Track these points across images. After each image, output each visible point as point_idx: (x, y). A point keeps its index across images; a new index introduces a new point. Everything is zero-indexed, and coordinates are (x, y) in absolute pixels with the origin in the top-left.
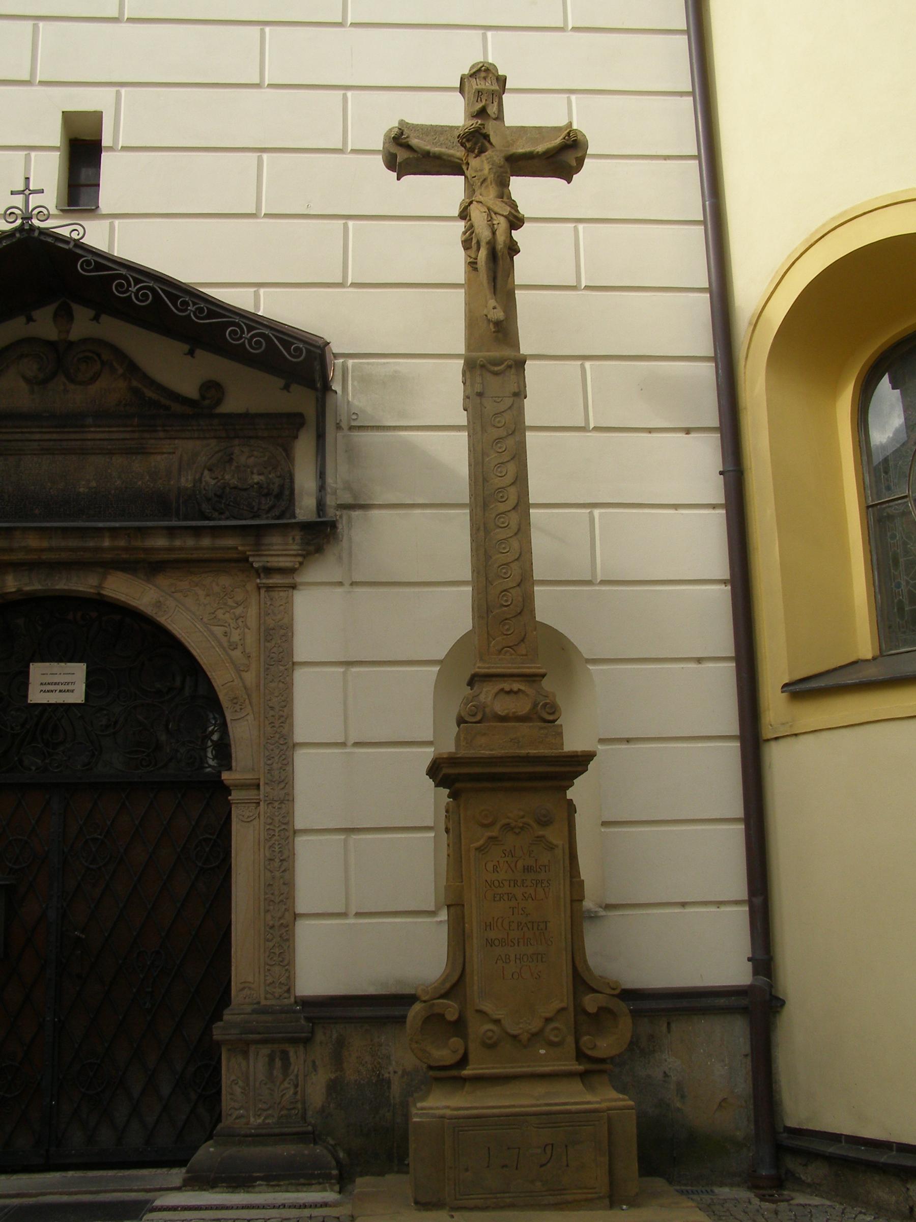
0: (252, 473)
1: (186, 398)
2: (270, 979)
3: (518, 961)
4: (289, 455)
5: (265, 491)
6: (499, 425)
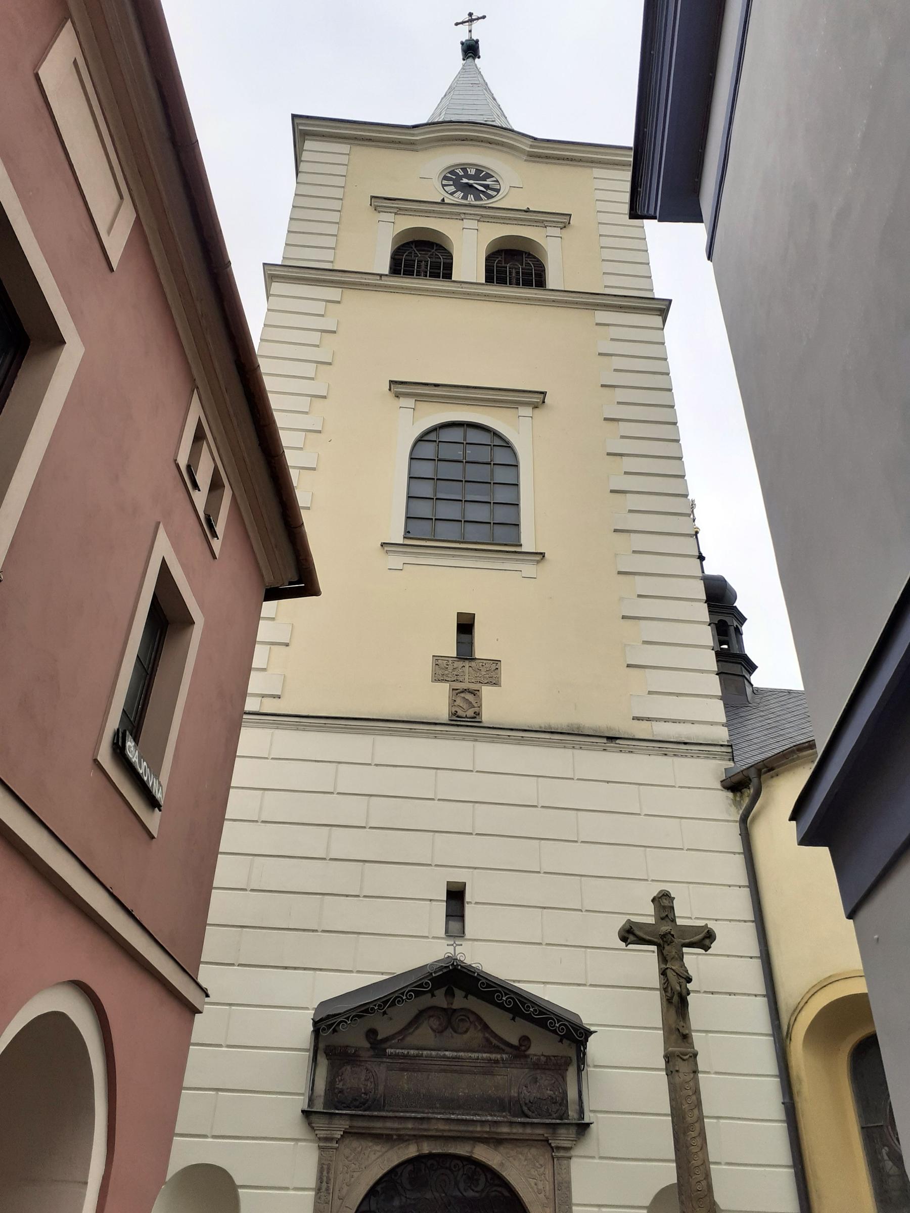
1: (512, 1044)
4: (564, 1078)
5: (555, 1100)
6: (688, 1088)
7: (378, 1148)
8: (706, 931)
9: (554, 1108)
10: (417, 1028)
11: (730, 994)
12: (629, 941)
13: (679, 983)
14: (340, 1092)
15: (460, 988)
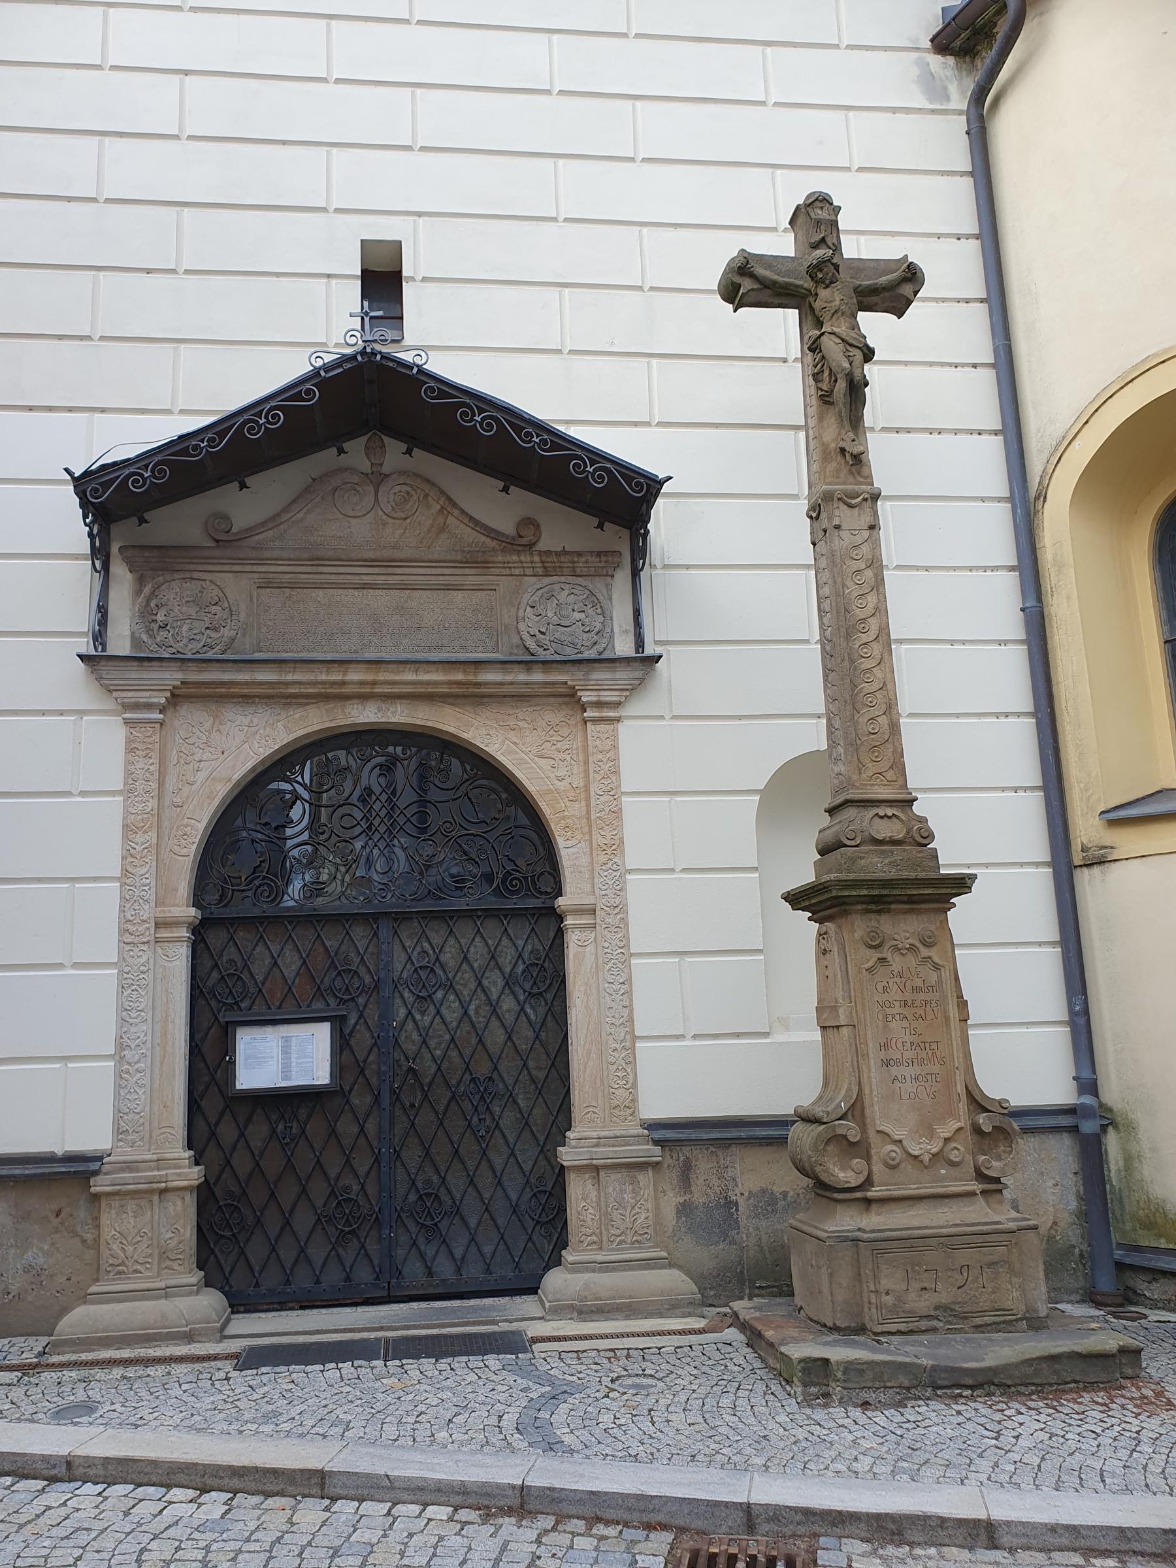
3: (914, 1081)
11: (931, 431)
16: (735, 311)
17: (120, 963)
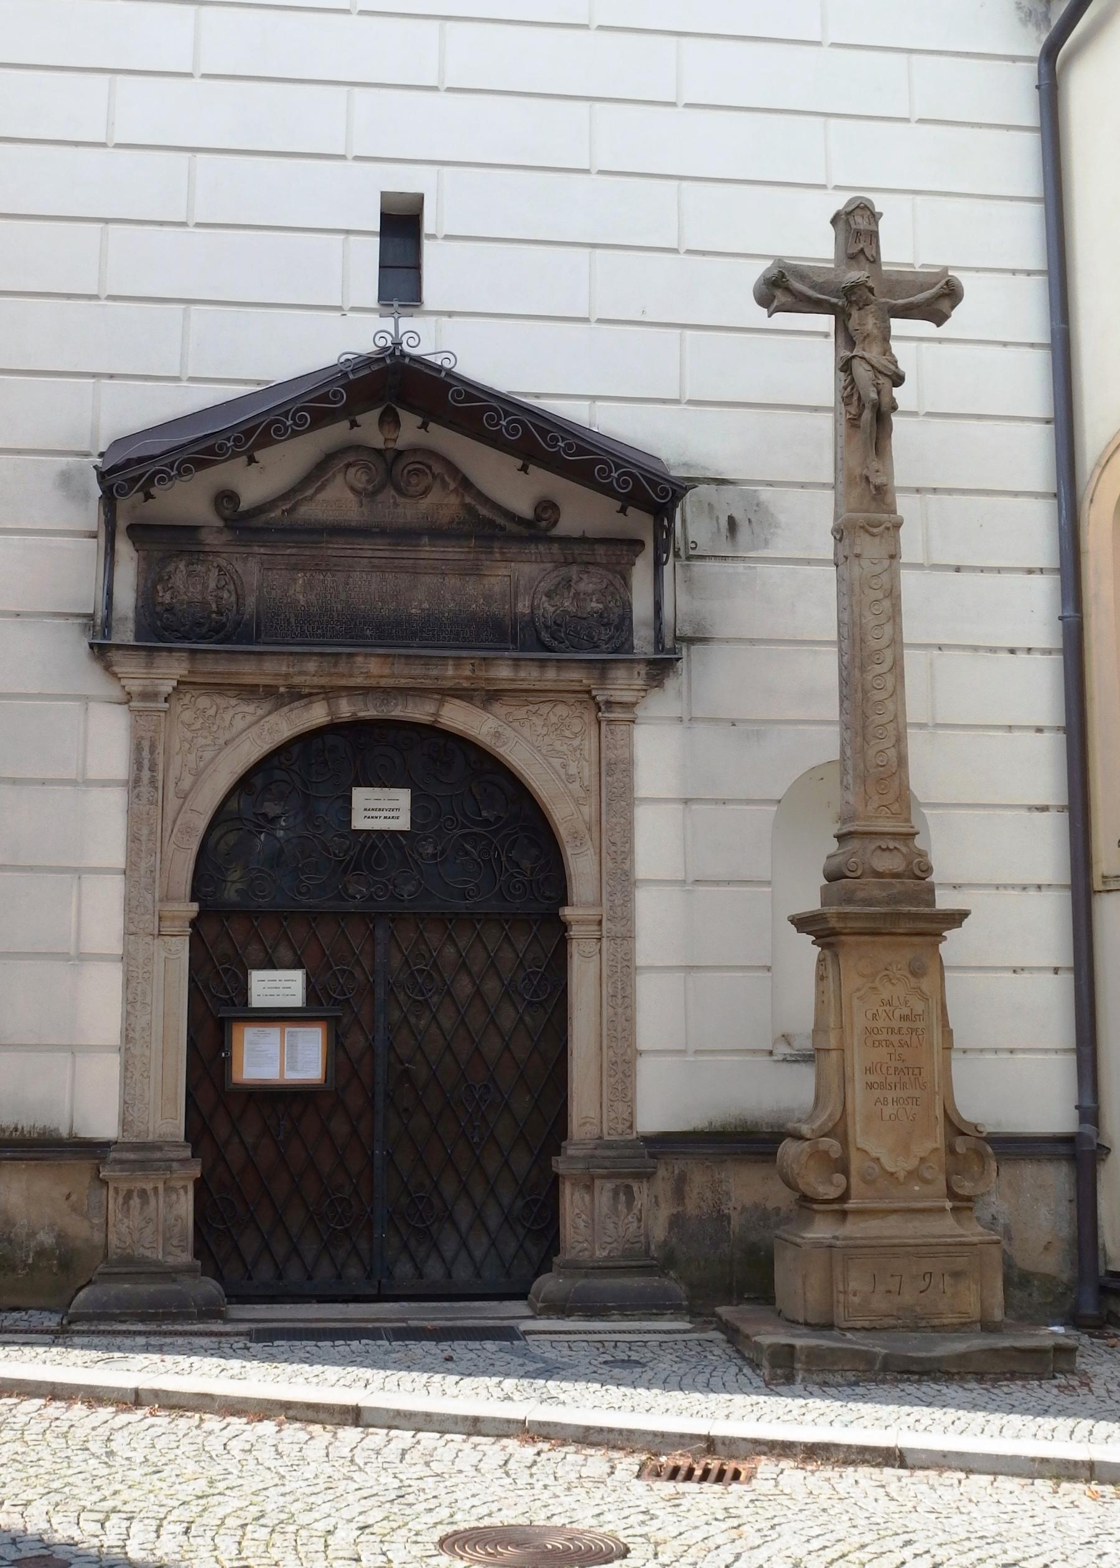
0: (591, 601)
1: (520, 518)
2: (613, 1115)
6: (876, 587)
7: (251, 709)
8: (944, 281)
9: (605, 634)
10: (319, 490)
12: (775, 303)
13: (877, 385)
14: (167, 610)
15: (412, 409)
16: (769, 316)
17: (126, 958)
